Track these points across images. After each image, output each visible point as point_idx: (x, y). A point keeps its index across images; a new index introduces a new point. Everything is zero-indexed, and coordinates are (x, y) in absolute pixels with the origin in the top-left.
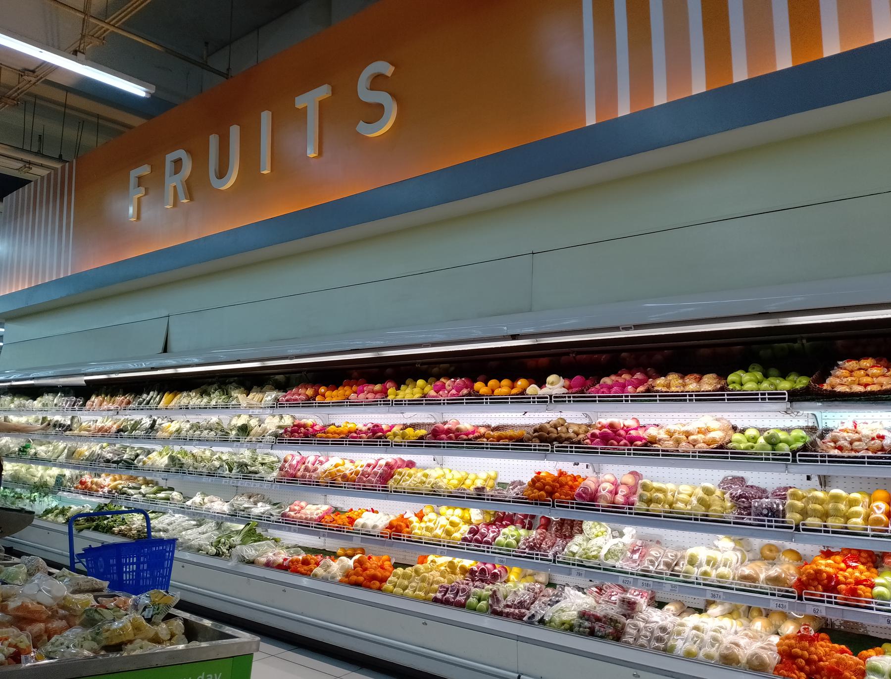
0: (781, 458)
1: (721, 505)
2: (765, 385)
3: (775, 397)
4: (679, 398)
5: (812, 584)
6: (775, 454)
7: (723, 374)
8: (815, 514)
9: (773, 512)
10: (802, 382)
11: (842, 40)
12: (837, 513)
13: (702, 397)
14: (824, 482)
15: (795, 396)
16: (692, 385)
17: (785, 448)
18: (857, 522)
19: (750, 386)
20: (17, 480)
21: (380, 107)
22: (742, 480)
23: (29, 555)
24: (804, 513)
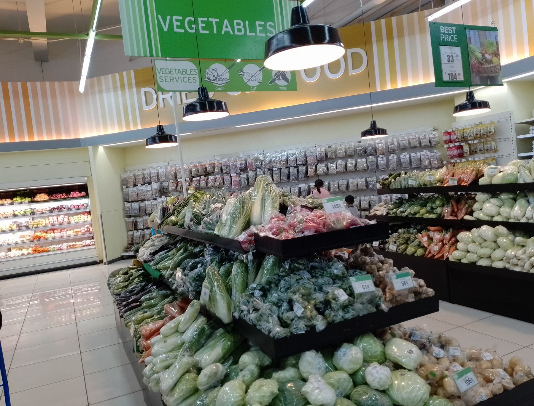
0: (28, 215)
1: (14, 227)
2: (23, 200)
3: (26, 203)
4: (20, 203)
5: (36, 238)
6: (25, 214)
7: (12, 199)
8: (35, 225)
9: (26, 226)
10: (30, 199)
11: (530, 52)
12: (39, 224)
13: (8, 204)
14: (33, 219)
15: (30, 202)
16: (6, 202)
17: (28, 213)
18: (44, 225)
19: (20, 201)
20: (37, 300)
21: (260, 33)
22: (17, 222)
23: (171, 365)
24: (33, 225)
